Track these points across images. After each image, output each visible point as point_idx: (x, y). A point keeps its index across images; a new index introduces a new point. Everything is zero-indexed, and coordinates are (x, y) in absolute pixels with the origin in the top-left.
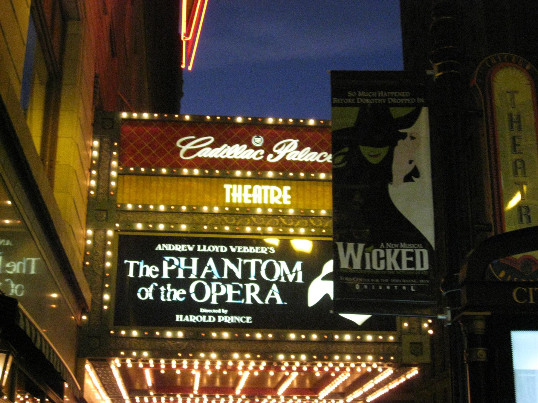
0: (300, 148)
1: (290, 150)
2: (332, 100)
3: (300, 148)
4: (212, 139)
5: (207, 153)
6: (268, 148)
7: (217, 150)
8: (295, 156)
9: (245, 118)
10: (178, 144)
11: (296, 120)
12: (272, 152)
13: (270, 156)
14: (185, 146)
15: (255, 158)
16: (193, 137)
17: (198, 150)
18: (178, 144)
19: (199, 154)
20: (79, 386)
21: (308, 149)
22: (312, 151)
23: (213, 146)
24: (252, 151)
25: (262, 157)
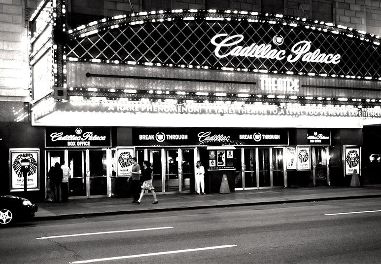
0: (312, 50)
1: (304, 52)
2: (79, 128)
3: (312, 50)
4: (62, 133)
5: (238, 52)
6: (287, 46)
7: (249, 48)
8: (309, 57)
9: (269, 14)
10: (213, 41)
11: (300, 19)
12: (291, 53)
13: (290, 56)
14: (218, 44)
15: (279, 59)
16: (226, 35)
17: (57, 138)
18: (213, 41)
19: (58, 139)
20: (83, 40)
21: (96, 135)
22: (321, 52)
23: (63, 136)
24: (76, 137)
25: (284, 57)
